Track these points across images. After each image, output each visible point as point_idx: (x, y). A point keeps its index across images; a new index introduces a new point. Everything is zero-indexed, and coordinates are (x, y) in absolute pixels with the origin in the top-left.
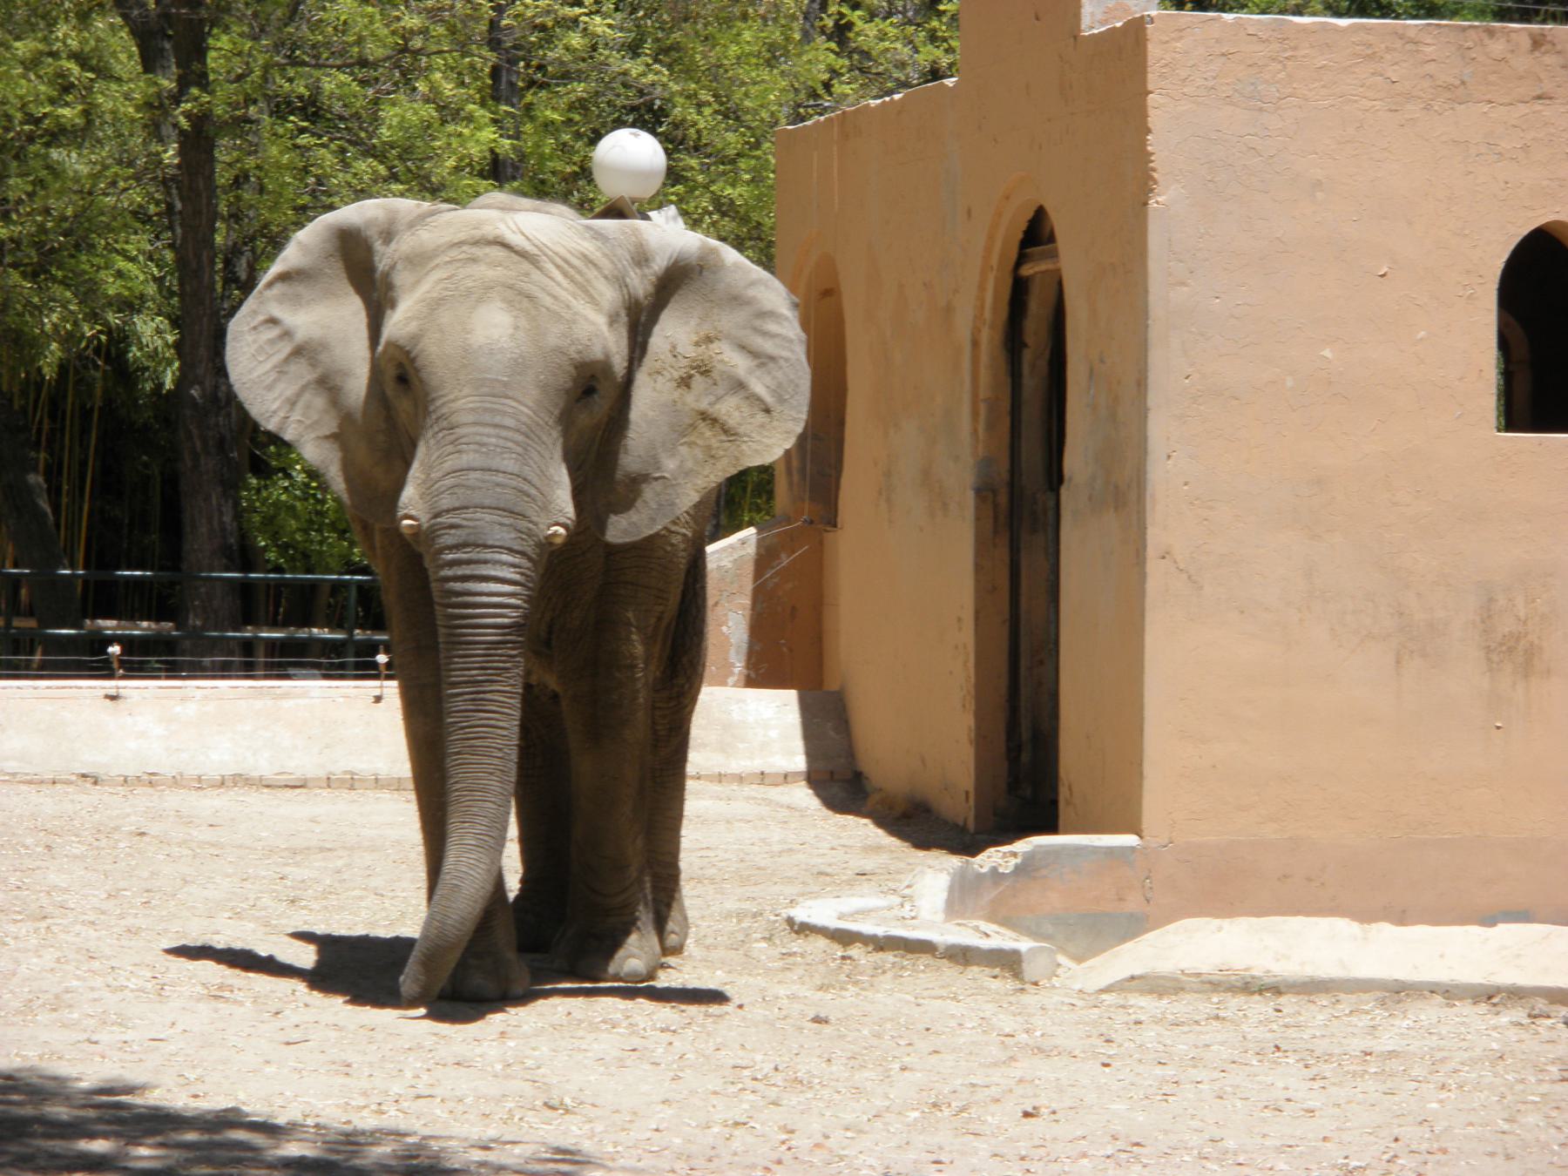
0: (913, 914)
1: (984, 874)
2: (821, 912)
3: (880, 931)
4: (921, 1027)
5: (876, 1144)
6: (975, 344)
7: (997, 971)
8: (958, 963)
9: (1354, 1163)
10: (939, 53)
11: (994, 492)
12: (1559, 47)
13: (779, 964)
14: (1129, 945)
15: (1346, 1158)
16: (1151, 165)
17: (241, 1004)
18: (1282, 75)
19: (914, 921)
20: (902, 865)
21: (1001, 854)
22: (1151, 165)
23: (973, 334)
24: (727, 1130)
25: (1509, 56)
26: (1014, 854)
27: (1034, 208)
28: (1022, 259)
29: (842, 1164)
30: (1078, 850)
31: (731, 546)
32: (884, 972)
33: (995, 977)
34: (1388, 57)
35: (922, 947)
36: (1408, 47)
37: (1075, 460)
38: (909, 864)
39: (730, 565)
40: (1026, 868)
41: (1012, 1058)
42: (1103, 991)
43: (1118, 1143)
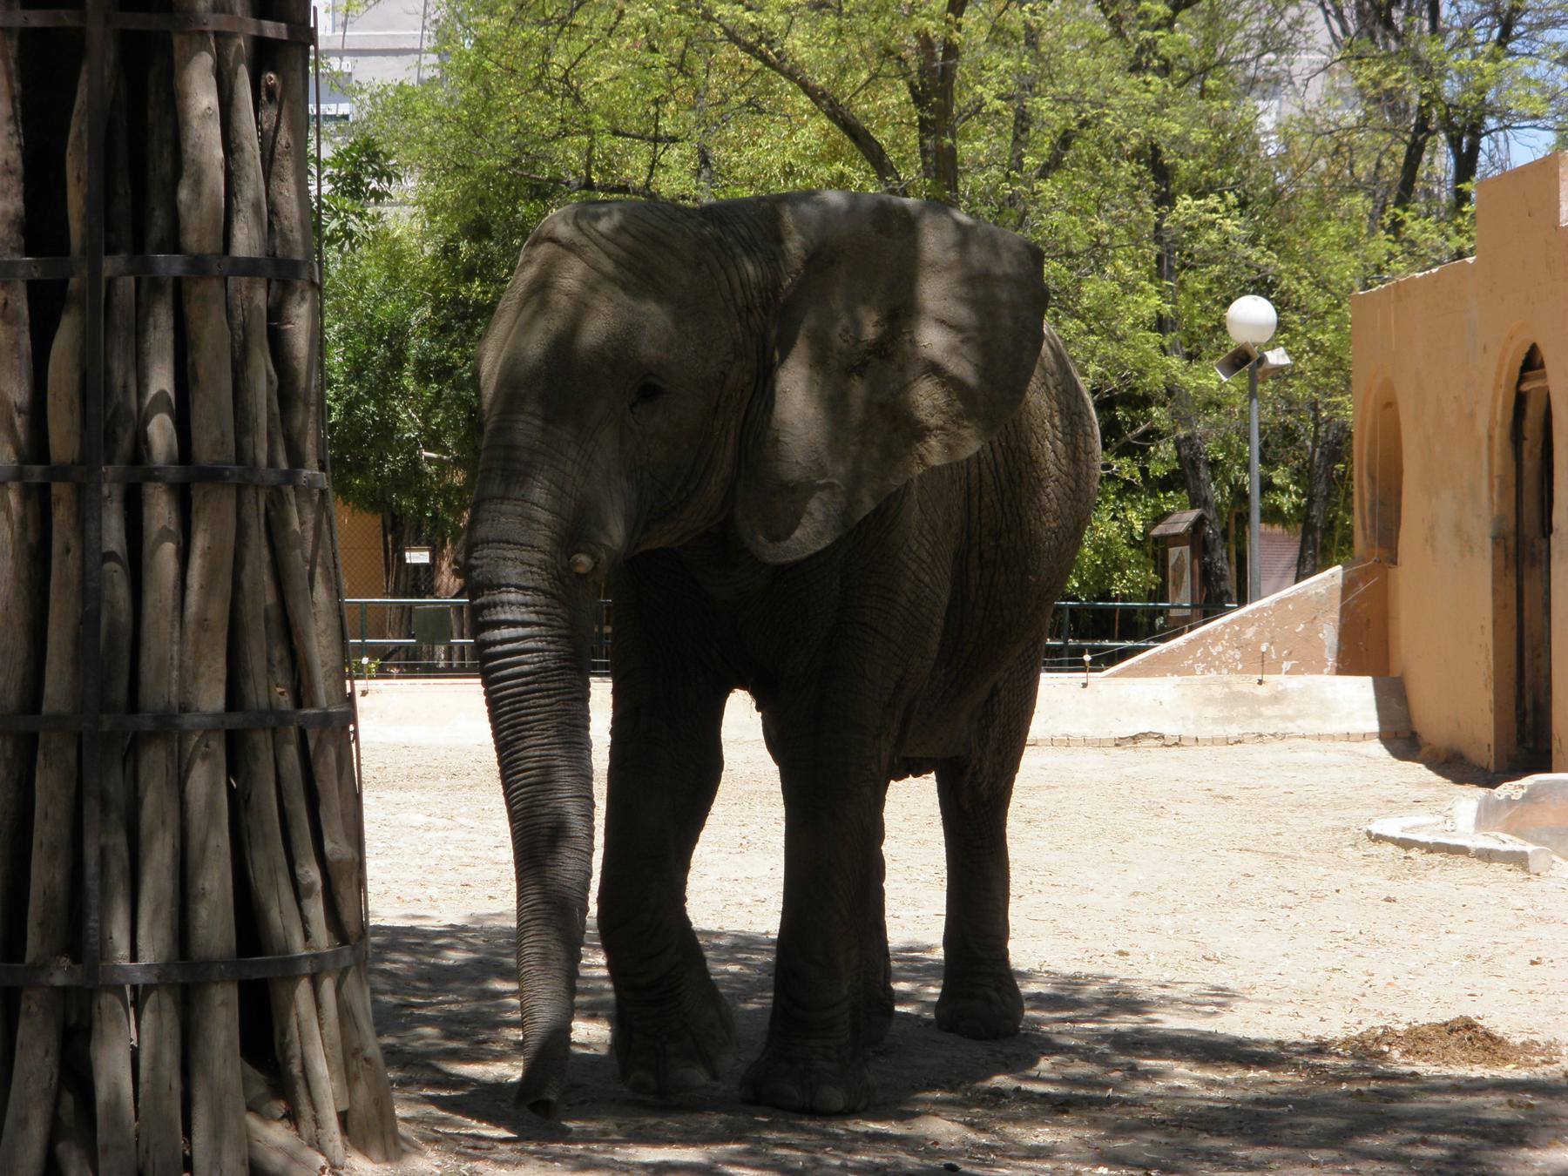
2: (1391, 826)
3: (1430, 840)
6: (1491, 438)
10: (1463, 240)
26: (1522, 787)
28: (1521, 380)
40: (1531, 796)
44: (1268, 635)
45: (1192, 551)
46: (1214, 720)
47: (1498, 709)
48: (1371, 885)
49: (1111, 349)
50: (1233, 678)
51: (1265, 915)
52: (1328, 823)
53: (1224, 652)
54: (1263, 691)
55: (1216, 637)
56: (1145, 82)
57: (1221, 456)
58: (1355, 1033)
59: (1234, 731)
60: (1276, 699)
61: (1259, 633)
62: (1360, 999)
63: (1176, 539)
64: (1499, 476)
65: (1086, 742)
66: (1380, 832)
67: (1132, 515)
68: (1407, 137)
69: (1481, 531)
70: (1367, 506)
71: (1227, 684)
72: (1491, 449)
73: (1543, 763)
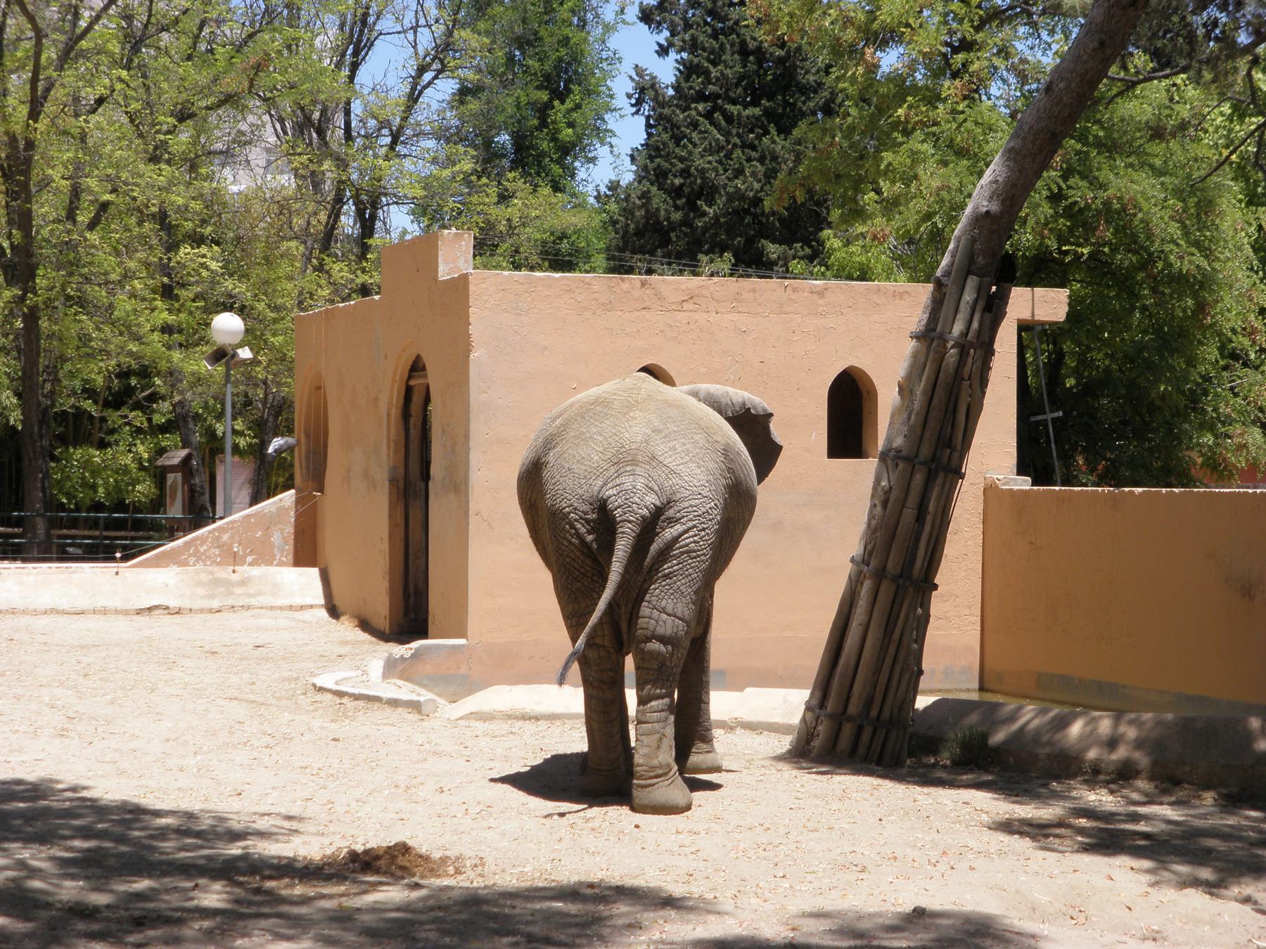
2: (327, 681)
3: (356, 691)
6: (389, 415)
10: (367, 278)
13: (311, 707)
14: (470, 697)
17: (73, 738)
28: (410, 377)
30: (439, 646)
35: (377, 699)
37: (435, 470)
40: (416, 655)
41: (425, 759)
42: (458, 719)
44: (237, 538)
45: (183, 477)
46: (203, 597)
47: (392, 592)
49: (133, 347)
50: (215, 569)
51: (255, 754)
52: (286, 674)
53: (208, 550)
54: (235, 577)
55: (203, 540)
56: (159, 169)
57: (200, 411)
58: (328, 852)
59: (215, 604)
60: (244, 582)
61: (231, 538)
63: (173, 469)
65: (117, 612)
67: (141, 448)
68: (329, 207)
69: (382, 476)
70: (303, 453)
71: (211, 573)
72: (389, 423)
73: (422, 632)
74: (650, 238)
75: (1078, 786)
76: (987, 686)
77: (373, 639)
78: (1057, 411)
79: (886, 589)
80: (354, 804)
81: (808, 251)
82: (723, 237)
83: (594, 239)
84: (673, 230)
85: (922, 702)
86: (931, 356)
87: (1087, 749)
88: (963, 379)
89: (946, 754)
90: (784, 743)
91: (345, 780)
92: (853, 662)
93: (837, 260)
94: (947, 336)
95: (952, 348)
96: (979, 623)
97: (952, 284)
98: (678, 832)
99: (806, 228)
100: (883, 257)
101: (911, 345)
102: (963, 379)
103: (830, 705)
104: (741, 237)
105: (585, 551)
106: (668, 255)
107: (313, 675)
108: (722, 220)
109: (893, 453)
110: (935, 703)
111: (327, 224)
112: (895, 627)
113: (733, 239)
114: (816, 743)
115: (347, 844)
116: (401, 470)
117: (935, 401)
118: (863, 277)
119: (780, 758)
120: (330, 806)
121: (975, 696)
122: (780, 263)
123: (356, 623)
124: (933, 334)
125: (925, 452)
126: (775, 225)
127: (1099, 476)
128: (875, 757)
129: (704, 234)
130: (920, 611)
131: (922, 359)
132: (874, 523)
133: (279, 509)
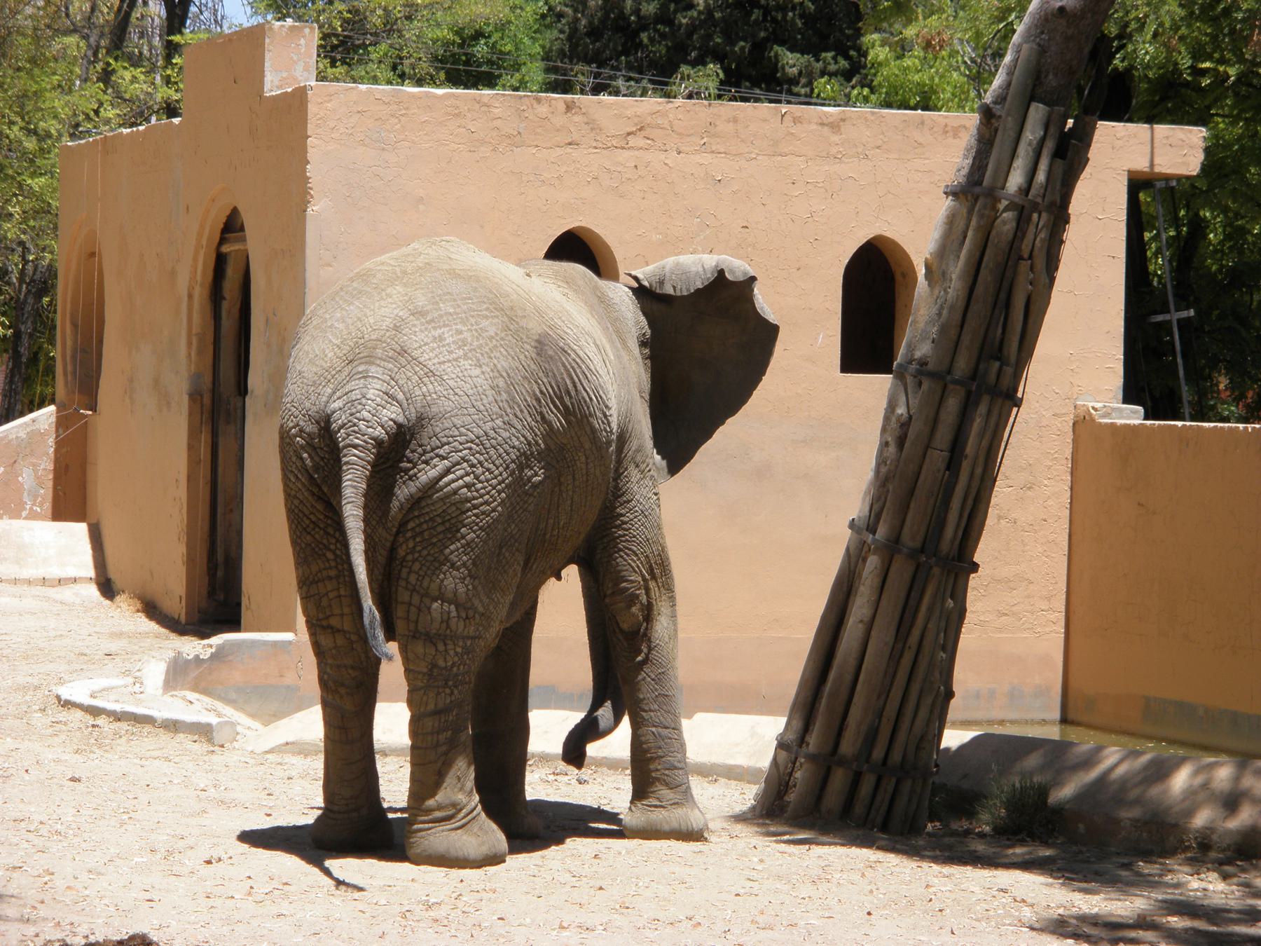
0: (141, 690)
1: (190, 660)
2: (78, 691)
3: (117, 707)
4: (143, 783)
5: (110, 885)
6: (190, 296)
7: (196, 737)
8: (170, 731)
9: (433, 900)
10: (171, 92)
11: (202, 396)
12: (583, 110)
13: (50, 731)
15: (427, 896)
16: (309, 185)
18: (398, 126)
19: (142, 695)
20: (136, 648)
21: (201, 646)
22: (309, 185)
23: (189, 290)
24: (8, 873)
25: (550, 116)
26: (211, 646)
27: (232, 208)
28: (222, 241)
29: (85, 903)
31: (25, 423)
32: (121, 737)
33: (195, 742)
34: (469, 115)
35: (147, 720)
36: (483, 109)
37: (256, 379)
38: (141, 647)
39: (25, 436)
40: (219, 655)
42: (267, 752)
43: (273, 882)
47: (190, 561)
48: (57, 761)
52: (21, 680)
62: (38, 905)
64: (196, 335)
66: (69, 698)
69: (179, 385)
70: (69, 353)
73: (232, 622)
74: (610, 40)
75: (1176, 867)
76: (1071, 715)
77: (163, 630)
78: (1187, 308)
79: (901, 570)
80: (84, 877)
81: (843, 63)
82: (719, 40)
83: (526, 40)
84: (644, 28)
85: (953, 738)
86: (974, 223)
87: (1190, 813)
88: (1021, 258)
89: (985, 816)
90: (746, 796)
91: (76, 840)
92: (848, 678)
93: (887, 79)
94: (1000, 193)
95: (1006, 209)
96: (1062, 623)
97: (1008, 115)
98: (562, 927)
99: (841, 31)
100: (955, 75)
101: (944, 205)
102: (1021, 258)
103: (813, 739)
104: (745, 40)
105: (315, 490)
106: (630, 67)
107: (61, 682)
108: (718, 15)
109: (914, 366)
110: (974, 741)
111: (120, 9)
112: (911, 626)
113: (733, 44)
114: (792, 797)
115: (60, 936)
116: (208, 379)
117: (979, 289)
118: (926, 104)
119: (740, 818)
120: (47, 879)
121: (1053, 733)
122: (803, 81)
123: (139, 606)
124: (977, 190)
125: (962, 365)
126: (796, 24)
127: (1247, 406)
128: (879, 820)
129: (690, 34)
130: (950, 603)
131: (960, 224)
132: (884, 470)
133: (31, 435)
